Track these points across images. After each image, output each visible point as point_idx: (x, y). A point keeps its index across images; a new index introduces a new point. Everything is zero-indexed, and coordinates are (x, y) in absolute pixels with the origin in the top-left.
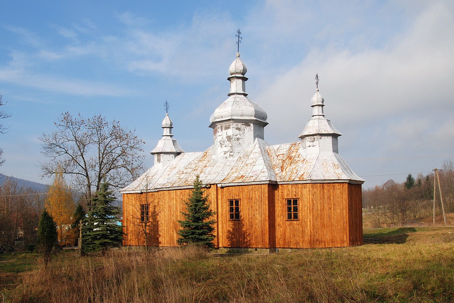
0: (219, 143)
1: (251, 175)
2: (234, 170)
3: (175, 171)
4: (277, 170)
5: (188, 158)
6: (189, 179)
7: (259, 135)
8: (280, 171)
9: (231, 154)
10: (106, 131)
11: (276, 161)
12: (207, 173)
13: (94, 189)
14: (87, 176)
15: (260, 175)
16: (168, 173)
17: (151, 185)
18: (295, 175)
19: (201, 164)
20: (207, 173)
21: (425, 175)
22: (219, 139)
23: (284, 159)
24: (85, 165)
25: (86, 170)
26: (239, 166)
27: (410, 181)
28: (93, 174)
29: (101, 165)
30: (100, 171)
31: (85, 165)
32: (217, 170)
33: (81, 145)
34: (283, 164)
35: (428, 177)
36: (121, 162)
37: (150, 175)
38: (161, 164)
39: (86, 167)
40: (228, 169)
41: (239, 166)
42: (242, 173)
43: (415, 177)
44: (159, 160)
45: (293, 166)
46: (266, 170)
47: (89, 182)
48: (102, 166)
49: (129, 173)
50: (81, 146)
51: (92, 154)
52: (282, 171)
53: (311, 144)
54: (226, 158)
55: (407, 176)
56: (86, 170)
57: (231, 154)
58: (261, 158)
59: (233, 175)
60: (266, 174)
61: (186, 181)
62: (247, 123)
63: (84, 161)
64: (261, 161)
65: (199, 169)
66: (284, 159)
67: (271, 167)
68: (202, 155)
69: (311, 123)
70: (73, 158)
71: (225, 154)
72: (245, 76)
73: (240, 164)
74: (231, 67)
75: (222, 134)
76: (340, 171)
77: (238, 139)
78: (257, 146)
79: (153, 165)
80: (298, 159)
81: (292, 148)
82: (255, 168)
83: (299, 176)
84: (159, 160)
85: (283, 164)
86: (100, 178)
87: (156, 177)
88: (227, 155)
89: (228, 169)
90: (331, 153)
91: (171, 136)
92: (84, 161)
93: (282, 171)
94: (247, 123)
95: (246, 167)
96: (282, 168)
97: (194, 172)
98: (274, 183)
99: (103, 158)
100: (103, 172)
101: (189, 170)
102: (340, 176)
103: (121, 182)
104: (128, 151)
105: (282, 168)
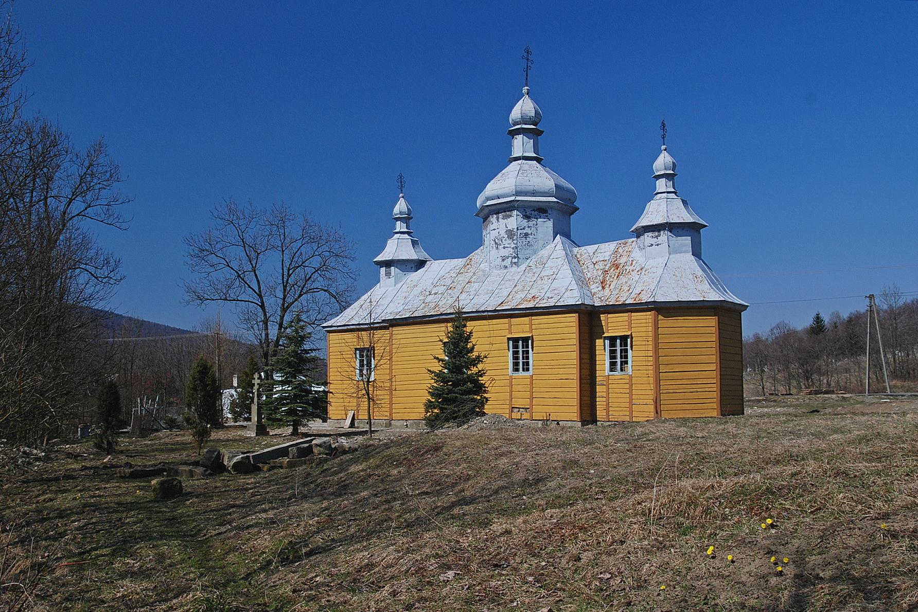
0: (493, 242)
1: (548, 294)
2: (519, 287)
3: (416, 291)
4: (595, 288)
5: (437, 269)
6: (441, 303)
7: (563, 230)
8: (600, 288)
9: (514, 260)
10: (294, 230)
11: (592, 273)
12: (472, 293)
13: (273, 332)
14: (262, 306)
15: (565, 296)
16: (405, 294)
17: (379, 310)
18: (628, 294)
19: (460, 278)
20: (472, 293)
21: (845, 315)
22: (494, 234)
23: (607, 268)
24: (260, 288)
25: (261, 297)
26: (529, 280)
27: (818, 323)
28: (273, 303)
29: (285, 287)
30: (285, 297)
31: (260, 288)
32: (491, 288)
33: (253, 252)
34: (604, 278)
35: (850, 320)
36: (320, 283)
37: (375, 298)
38: (392, 280)
39: (260, 292)
40: (508, 286)
41: (529, 280)
42: (533, 292)
43: (827, 319)
44: (388, 274)
45: (623, 279)
46: (575, 287)
47: (265, 315)
48: (288, 288)
49: (333, 300)
50: (253, 255)
51: (270, 268)
52: (603, 288)
53: (654, 241)
54: (506, 267)
55: (814, 315)
56: (261, 297)
57: (514, 260)
58: (566, 266)
59: (518, 296)
60: (576, 293)
61: (437, 306)
62: (541, 210)
63: (258, 281)
64: (566, 271)
65: (459, 287)
66: (607, 268)
67: (583, 282)
68: (463, 263)
69: (652, 206)
70: (239, 276)
71: (503, 260)
72: (540, 127)
73: (530, 278)
74: (513, 112)
75: (498, 226)
76: (706, 286)
77: (526, 235)
78: (560, 246)
79: (379, 281)
80: (631, 268)
81: (620, 250)
82: (556, 284)
83: (633, 295)
84: (388, 274)
85: (604, 278)
86: (284, 310)
87: (385, 302)
88: (508, 262)
89: (508, 286)
90: (689, 256)
91: (409, 233)
92: (258, 281)
93: (603, 288)
94: (541, 210)
95: (540, 282)
96: (603, 284)
97: (450, 291)
98: (589, 308)
99: (289, 276)
100: (289, 300)
101: (441, 289)
102: (706, 295)
103: (320, 317)
104: (332, 262)
105: (603, 284)
